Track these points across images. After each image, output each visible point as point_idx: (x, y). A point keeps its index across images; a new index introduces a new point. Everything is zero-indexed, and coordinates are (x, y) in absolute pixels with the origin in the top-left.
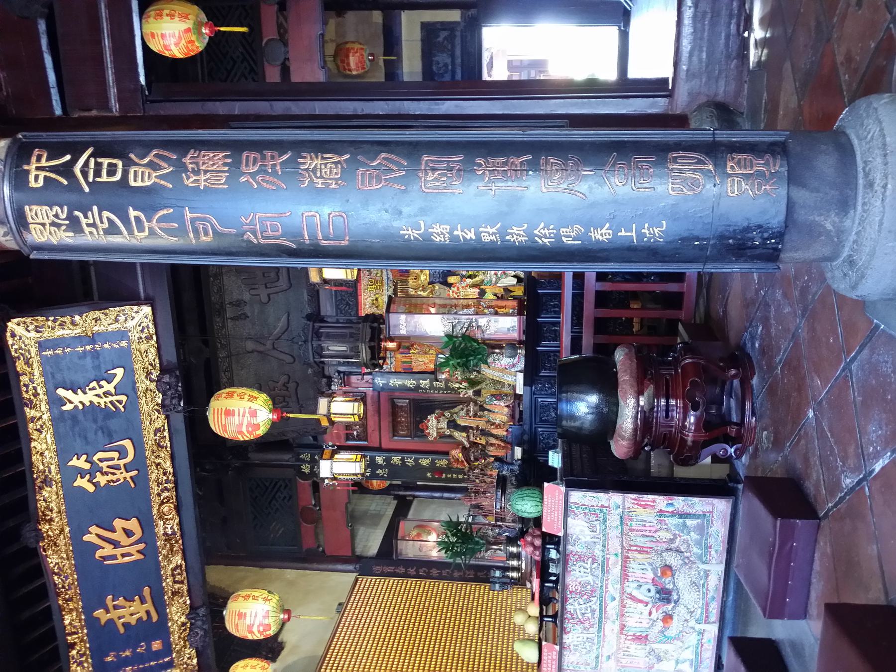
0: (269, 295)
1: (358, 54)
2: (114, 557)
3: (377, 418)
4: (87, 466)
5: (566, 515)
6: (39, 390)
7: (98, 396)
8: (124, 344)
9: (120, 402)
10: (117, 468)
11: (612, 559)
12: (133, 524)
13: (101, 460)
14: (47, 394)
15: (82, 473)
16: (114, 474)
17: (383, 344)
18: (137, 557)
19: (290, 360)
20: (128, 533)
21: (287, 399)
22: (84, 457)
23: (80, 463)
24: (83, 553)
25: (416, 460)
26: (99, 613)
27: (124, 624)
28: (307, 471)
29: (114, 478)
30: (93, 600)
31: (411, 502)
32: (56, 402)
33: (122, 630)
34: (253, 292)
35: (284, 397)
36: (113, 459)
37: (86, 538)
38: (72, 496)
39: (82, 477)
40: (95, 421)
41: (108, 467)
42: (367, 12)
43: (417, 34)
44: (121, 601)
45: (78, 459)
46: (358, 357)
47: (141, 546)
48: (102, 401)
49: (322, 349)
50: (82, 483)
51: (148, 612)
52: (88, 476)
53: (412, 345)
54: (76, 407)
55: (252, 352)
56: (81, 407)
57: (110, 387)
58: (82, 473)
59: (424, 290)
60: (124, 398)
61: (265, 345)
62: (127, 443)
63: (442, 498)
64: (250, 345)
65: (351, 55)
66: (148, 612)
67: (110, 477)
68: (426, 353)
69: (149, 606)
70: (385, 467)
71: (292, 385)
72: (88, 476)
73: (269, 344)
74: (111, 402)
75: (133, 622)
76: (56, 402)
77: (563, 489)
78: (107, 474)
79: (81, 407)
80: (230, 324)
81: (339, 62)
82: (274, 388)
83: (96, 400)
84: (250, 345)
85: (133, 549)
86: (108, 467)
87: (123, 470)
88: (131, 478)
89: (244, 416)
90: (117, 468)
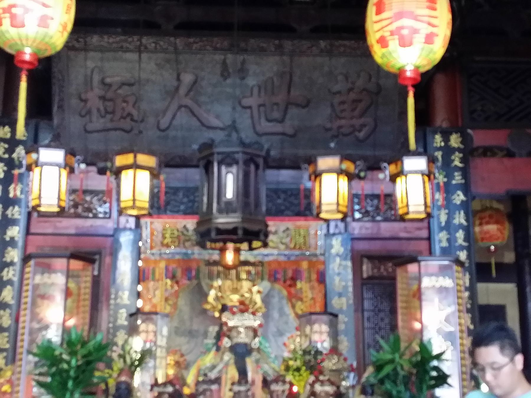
0: (250, 107)
1: (499, 234)
3: (73, 231)
17: (231, 246)
19: (163, 125)
21: (109, 116)
25: (10, 282)
34: (256, 91)
35: (113, 112)
46: (220, 211)
49: (229, 165)
53: (177, 283)
55: (178, 79)
59: (217, 298)
61: (187, 95)
64: (187, 78)
65: (499, 226)
68: (167, 300)
71: (127, 124)
73: (188, 101)
80: (219, 57)
81: (488, 213)
82: (125, 101)
84: (187, 78)
89: (430, 24)
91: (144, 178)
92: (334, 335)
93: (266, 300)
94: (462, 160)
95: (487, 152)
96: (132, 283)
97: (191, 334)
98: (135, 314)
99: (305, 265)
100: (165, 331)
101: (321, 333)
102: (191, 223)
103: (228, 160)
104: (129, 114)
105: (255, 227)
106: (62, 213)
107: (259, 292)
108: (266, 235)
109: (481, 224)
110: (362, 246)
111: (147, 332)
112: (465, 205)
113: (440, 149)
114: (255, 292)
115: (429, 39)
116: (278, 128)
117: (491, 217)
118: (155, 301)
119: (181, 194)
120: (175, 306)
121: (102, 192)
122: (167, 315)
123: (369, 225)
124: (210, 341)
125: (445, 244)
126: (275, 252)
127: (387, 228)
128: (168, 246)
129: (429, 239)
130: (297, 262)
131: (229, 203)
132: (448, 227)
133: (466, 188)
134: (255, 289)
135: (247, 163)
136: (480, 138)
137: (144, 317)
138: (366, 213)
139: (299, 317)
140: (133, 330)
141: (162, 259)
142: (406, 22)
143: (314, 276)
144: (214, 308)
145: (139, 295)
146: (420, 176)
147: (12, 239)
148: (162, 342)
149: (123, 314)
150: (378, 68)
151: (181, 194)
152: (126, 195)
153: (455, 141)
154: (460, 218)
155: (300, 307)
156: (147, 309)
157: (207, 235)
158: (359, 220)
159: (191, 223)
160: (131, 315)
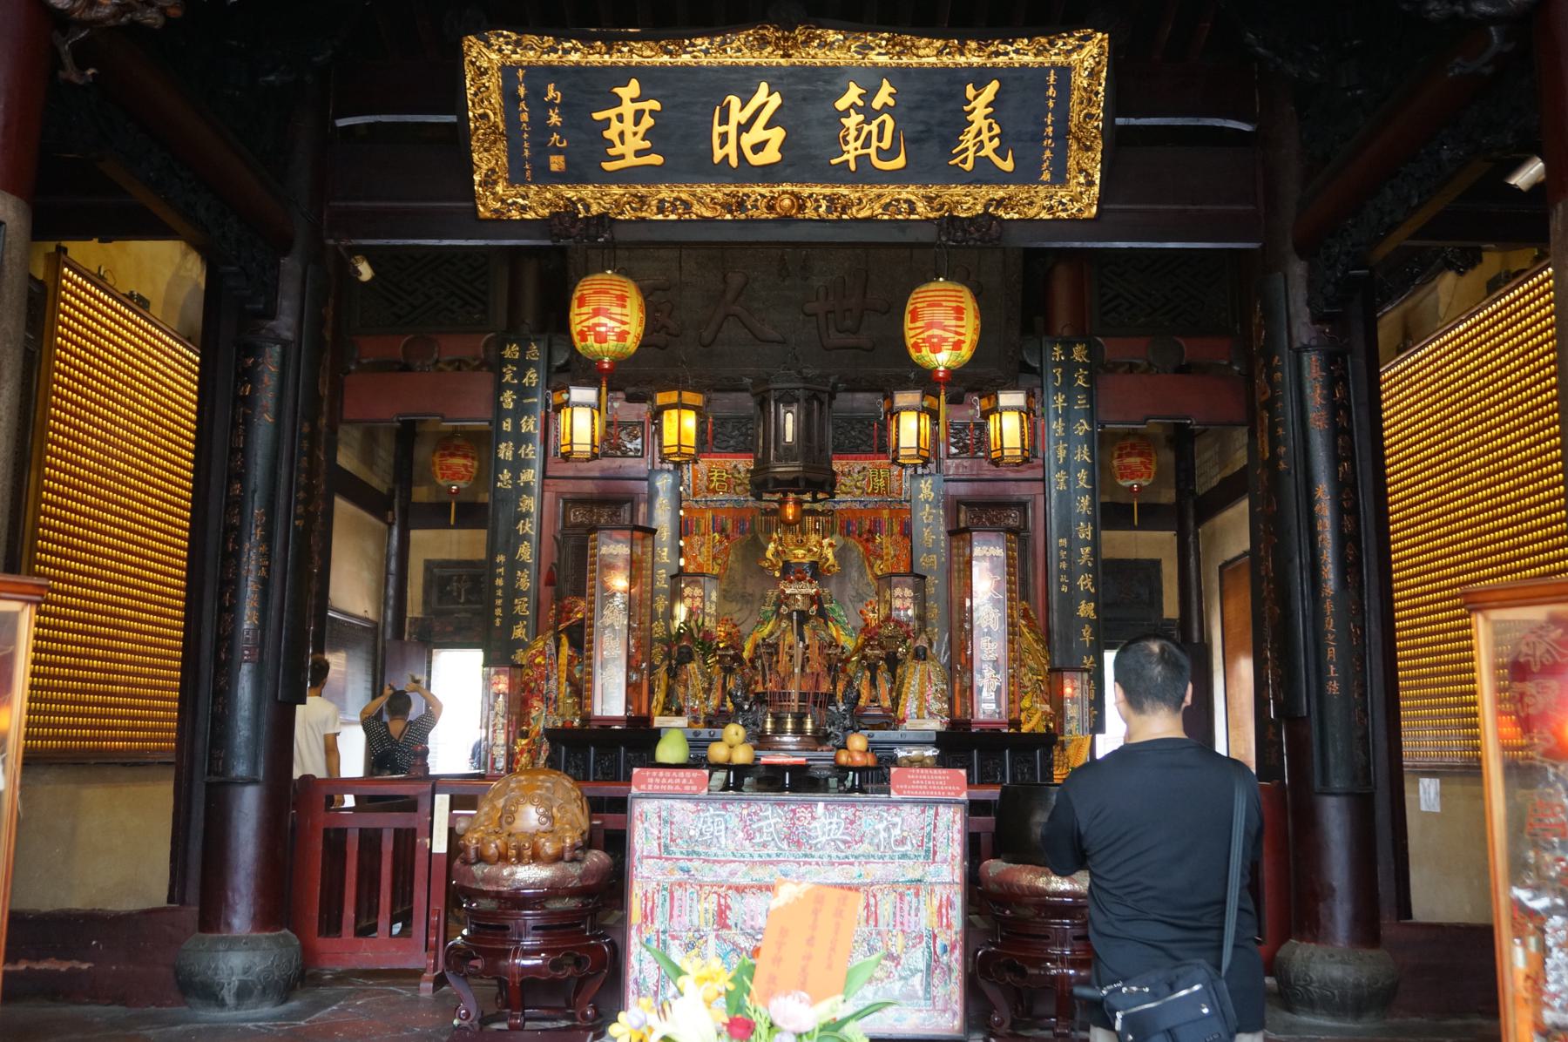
0: (815, 315)
2: (724, 120)
3: (597, 474)
4: (877, 104)
5: (915, 802)
6: (1001, 58)
7: (979, 133)
8: (1046, 176)
9: (964, 161)
10: (866, 144)
11: (856, 870)
12: (771, 155)
13: (881, 127)
14: (994, 67)
15: (869, 96)
16: (857, 139)
17: (791, 496)
18: (718, 155)
20: (758, 148)
22: (891, 102)
23: (884, 96)
24: (743, 81)
26: (634, 88)
27: (608, 120)
28: (507, 353)
29: (850, 138)
30: (652, 80)
31: (383, 518)
32: (980, 77)
33: (597, 116)
36: (880, 139)
37: (764, 87)
38: (833, 79)
39: (860, 96)
40: (942, 124)
41: (870, 133)
42: (1173, 480)
43: (1145, 554)
44: (648, 121)
45: (891, 95)
46: (778, 459)
47: (734, 162)
48: (970, 136)
49: (788, 403)
50: (853, 94)
51: (622, 157)
52: (860, 103)
53: (727, 537)
54: (969, 102)
56: (967, 108)
57: (988, 151)
58: (869, 96)
59: (777, 553)
60: (969, 166)
62: (899, 162)
63: (388, 573)
64: (736, 280)
66: (622, 157)
67: (853, 133)
68: (714, 558)
69: (631, 161)
70: (516, 485)
72: (860, 103)
73: (737, 309)
74: (967, 149)
75: (607, 134)
76: (980, 77)
77: (964, 796)
78: (859, 131)
79: (967, 108)
81: (1131, 441)
83: (973, 129)
84: (736, 280)
85: (731, 148)
86: (870, 133)
87: (861, 152)
88: (847, 161)
89: (957, 333)
90: (866, 144)
91: (690, 420)
92: (921, 600)
93: (841, 554)
94: (1088, 379)
95: (1113, 368)
96: (673, 537)
97: (746, 599)
98: (678, 575)
99: (885, 514)
100: (714, 596)
101: (904, 598)
102: (744, 464)
103: (788, 399)
104: (664, 326)
105: (820, 477)
106: (594, 457)
107: (831, 545)
108: (833, 485)
109: (1120, 456)
110: (962, 489)
111: (693, 597)
112: (1089, 437)
113: (1058, 364)
114: (827, 549)
115: (957, 346)
116: (851, 340)
117: (1133, 446)
118: (700, 559)
119: (730, 426)
120: (724, 566)
121: (631, 424)
122: (716, 577)
123: (966, 463)
124: (769, 608)
125: (1062, 487)
126: (848, 498)
127: (988, 471)
128: (715, 492)
129: (1043, 480)
130: (877, 510)
131: (789, 448)
132: (1066, 466)
133: (1091, 416)
134: (826, 542)
135: (808, 400)
136: (1113, 349)
137: (689, 579)
138: (964, 448)
139: (878, 578)
140: (676, 595)
141: (708, 507)
142: (936, 332)
143: (896, 529)
144: (773, 565)
145: (681, 552)
146: (1016, 415)
147: (527, 483)
148: (711, 609)
149: (662, 574)
150: (964, 281)
151: (730, 426)
152: (670, 437)
153: (1079, 354)
154: (1082, 454)
155: (880, 567)
156: (691, 569)
157: (761, 483)
158: (955, 456)
159: (744, 464)
160: (672, 577)
